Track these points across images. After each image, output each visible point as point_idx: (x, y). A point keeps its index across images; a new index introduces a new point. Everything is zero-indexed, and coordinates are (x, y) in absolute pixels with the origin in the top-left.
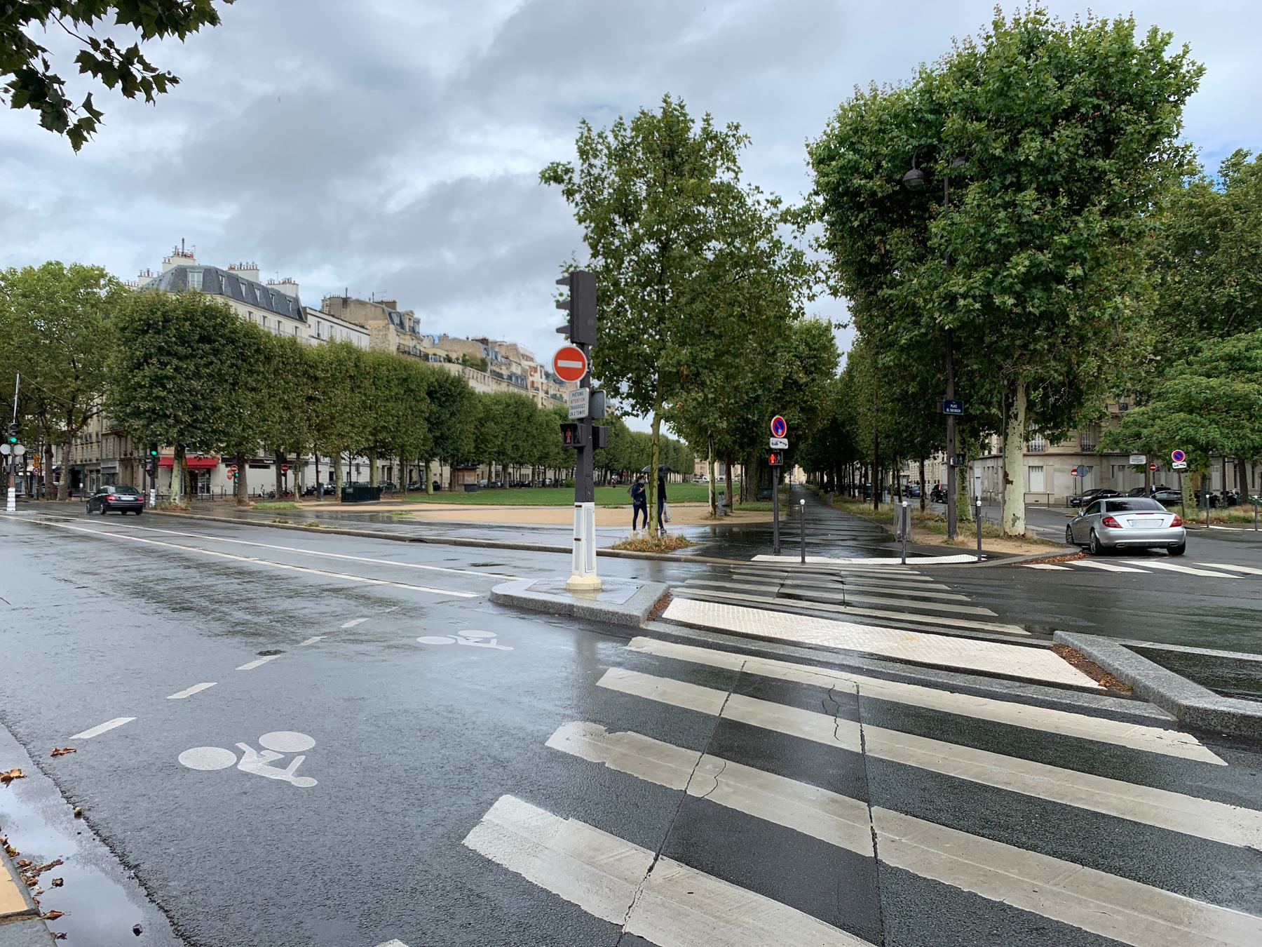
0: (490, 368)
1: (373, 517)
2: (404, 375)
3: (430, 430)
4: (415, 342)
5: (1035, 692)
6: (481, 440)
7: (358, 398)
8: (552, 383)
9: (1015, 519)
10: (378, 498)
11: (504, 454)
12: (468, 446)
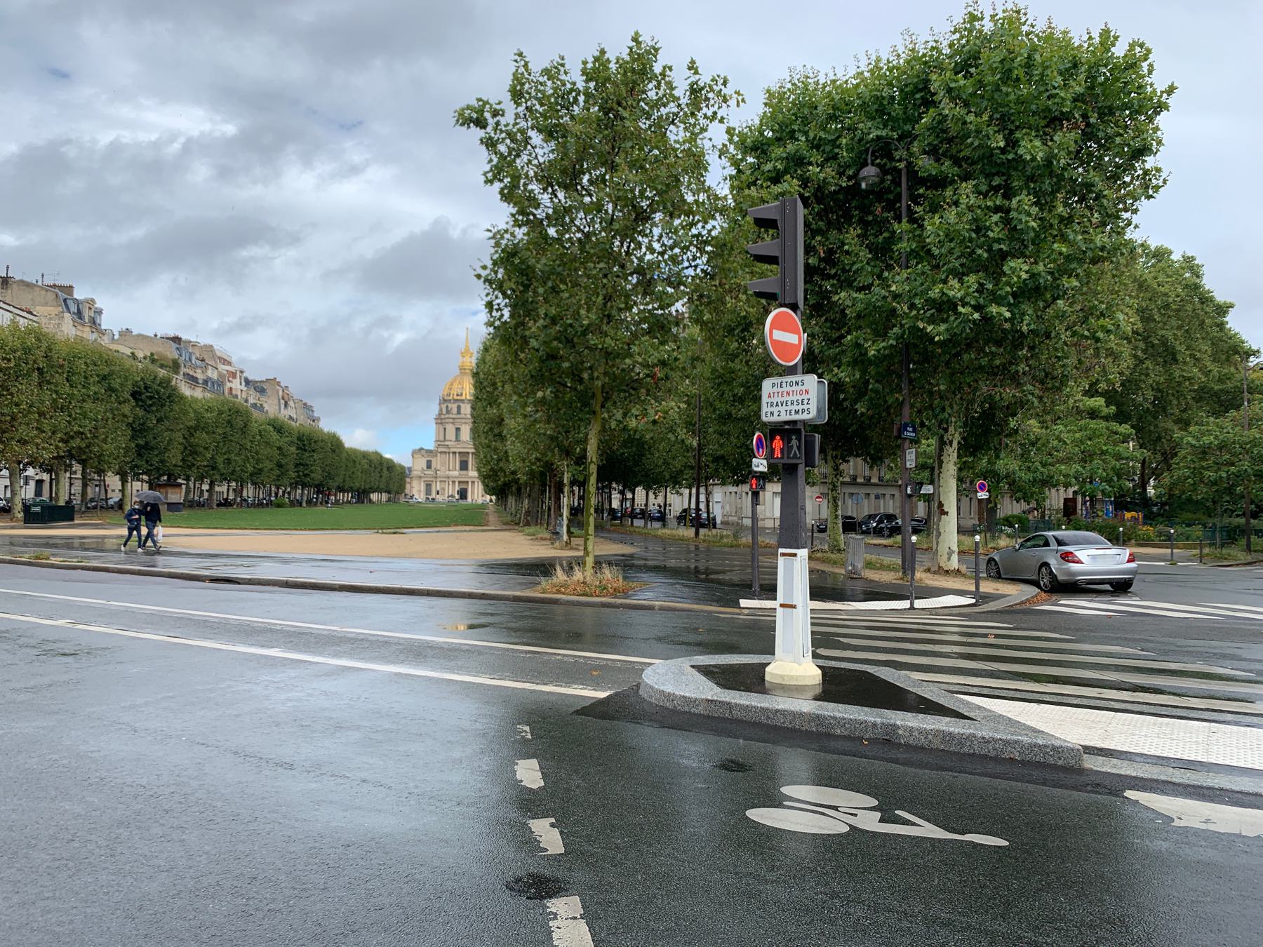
0: (183, 370)
1: (68, 544)
2: (106, 371)
3: (133, 438)
4: (95, 336)
5: (1114, 766)
6: (191, 451)
7: (47, 397)
8: (252, 392)
9: (950, 553)
10: (72, 519)
11: (214, 468)
12: (174, 457)
